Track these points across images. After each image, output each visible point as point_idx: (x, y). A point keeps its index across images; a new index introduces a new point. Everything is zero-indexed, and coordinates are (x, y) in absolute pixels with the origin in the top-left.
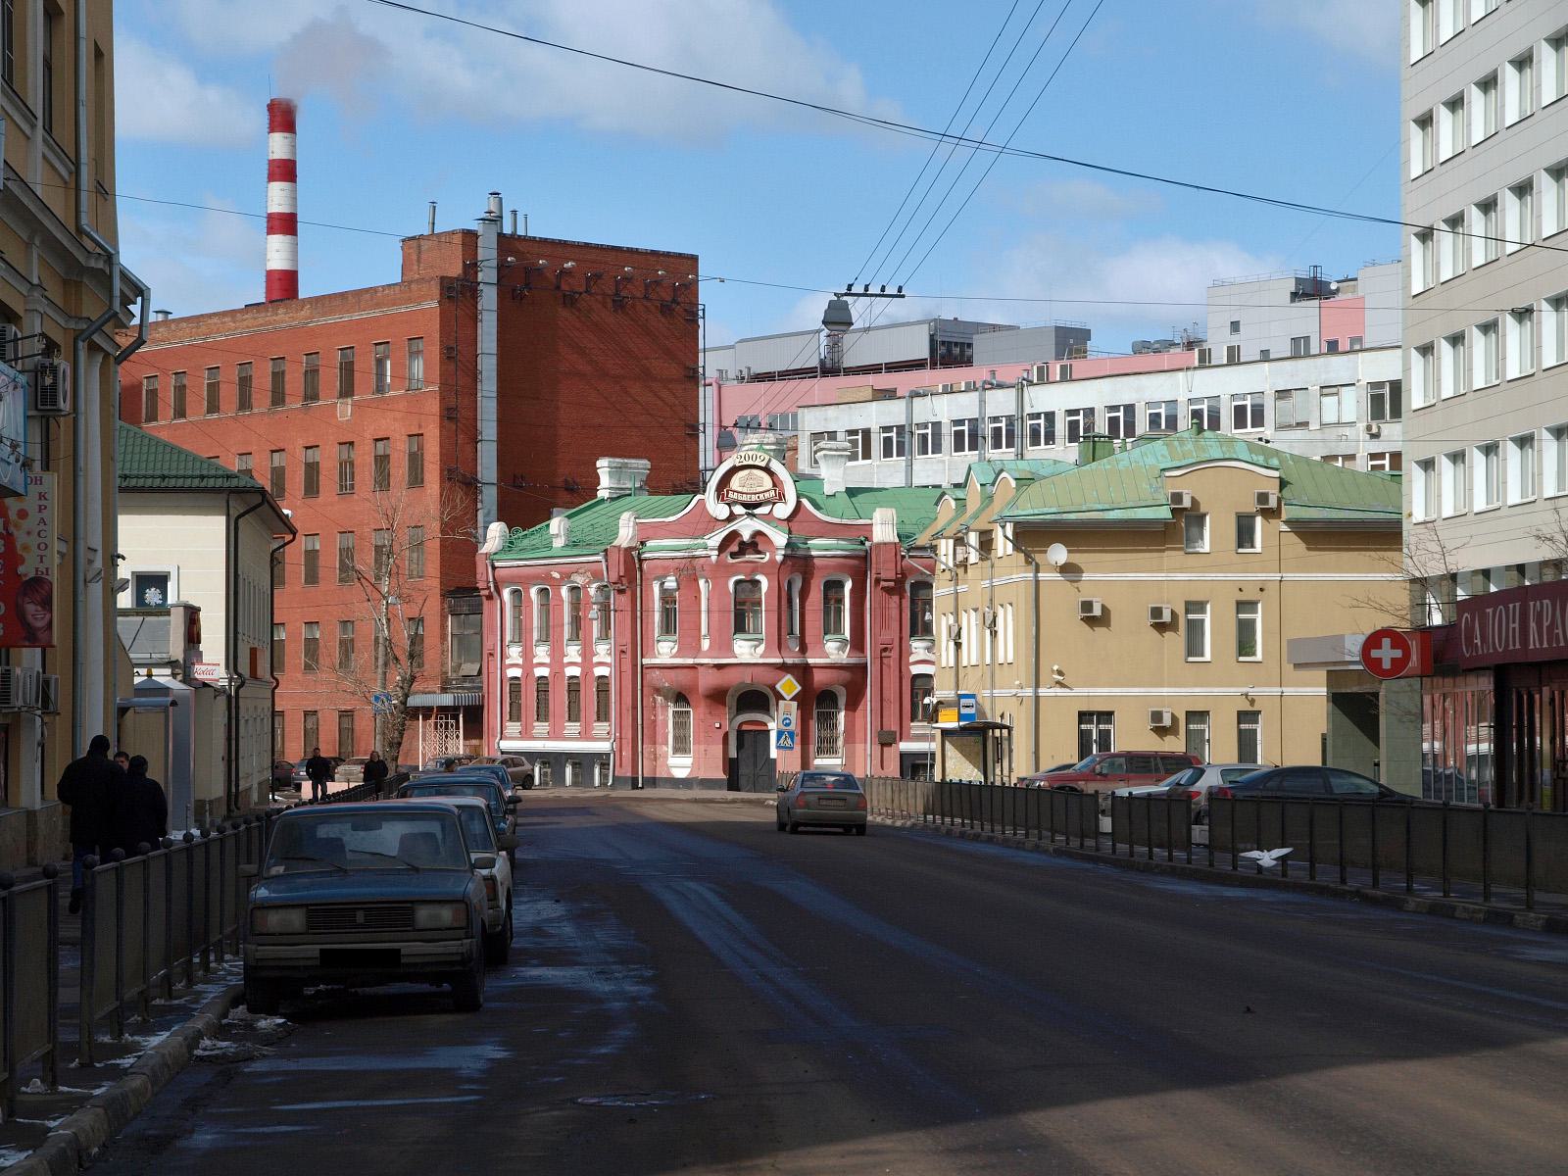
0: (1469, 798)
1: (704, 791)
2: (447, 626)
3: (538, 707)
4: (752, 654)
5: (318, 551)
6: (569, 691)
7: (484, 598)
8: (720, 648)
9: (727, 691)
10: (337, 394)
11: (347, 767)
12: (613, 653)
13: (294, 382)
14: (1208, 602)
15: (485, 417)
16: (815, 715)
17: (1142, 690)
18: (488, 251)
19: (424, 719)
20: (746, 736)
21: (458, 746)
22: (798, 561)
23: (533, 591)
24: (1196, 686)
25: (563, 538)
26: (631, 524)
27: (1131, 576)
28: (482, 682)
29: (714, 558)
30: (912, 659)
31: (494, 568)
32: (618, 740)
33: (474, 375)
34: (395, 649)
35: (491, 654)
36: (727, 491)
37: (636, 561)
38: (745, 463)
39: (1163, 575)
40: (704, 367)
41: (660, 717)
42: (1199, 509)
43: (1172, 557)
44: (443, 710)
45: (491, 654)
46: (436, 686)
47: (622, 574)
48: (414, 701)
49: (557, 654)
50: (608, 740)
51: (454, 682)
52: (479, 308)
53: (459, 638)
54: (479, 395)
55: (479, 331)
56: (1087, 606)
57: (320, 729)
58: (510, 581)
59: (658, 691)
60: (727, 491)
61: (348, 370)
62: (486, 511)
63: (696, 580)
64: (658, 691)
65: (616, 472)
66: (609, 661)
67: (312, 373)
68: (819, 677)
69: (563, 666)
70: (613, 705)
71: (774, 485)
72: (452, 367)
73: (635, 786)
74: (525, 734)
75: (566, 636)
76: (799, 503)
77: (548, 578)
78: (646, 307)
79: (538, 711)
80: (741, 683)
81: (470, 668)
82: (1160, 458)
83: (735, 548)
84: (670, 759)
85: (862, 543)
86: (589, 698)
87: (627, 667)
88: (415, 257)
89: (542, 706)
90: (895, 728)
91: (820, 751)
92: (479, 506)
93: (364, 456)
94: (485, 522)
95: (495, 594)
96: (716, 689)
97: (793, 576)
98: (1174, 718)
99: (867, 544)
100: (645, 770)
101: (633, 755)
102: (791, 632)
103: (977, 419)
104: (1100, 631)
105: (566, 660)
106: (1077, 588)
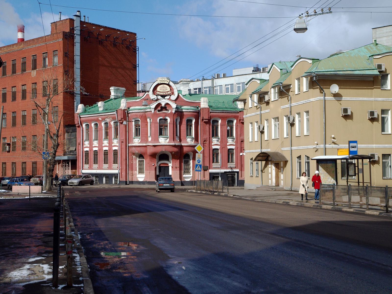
0: (41, 175)
1: (149, 185)
2: (65, 136)
3: (94, 160)
4: (165, 142)
5: (26, 115)
6: (104, 155)
7: (77, 127)
8: (155, 140)
9: (157, 154)
10: (31, 69)
11: (34, 179)
12: (119, 142)
13: (19, 67)
14: (389, 110)
15: (77, 74)
16: (183, 161)
17: (366, 145)
18: (77, 24)
19: (58, 164)
20: (162, 168)
21: (69, 172)
22: (179, 113)
23: (93, 125)
24: (386, 144)
25: (102, 108)
26: (125, 102)
27: (361, 99)
28: (76, 153)
29: (153, 112)
30: (213, 144)
31: (80, 118)
32: (121, 170)
33: (73, 62)
34: (51, 133)
35: (79, 144)
36: (156, 91)
37: (127, 114)
38: (162, 83)
39: (373, 98)
40: (138, 64)
41: (134, 162)
42: (386, 73)
43: (376, 91)
44: (64, 161)
45: (79, 144)
46: (62, 154)
47: (122, 117)
48: (57, 158)
49: (100, 144)
50: (117, 169)
51: (67, 153)
52: (75, 42)
53: (69, 140)
54: (75, 67)
55: (75, 49)
56: (345, 110)
57: (26, 167)
58: (85, 121)
59: (134, 154)
60: (156, 91)
61: (35, 61)
62: (77, 102)
63: (146, 119)
64: (134, 154)
65: (116, 91)
66: (118, 145)
67: (24, 64)
68: (185, 149)
69: (102, 147)
70: (119, 159)
71: (171, 90)
72: (67, 59)
73: (126, 184)
74: (90, 168)
75: (103, 138)
76: (178, 95)
77: (98, 120)
78: (122, 46)
79: (94, 161)
80: (162, 151)
81: (72, 149)
82: (365, 53)
83: (159, 109)
84: (137, 175)
85: (198, 108)
86: (111, 157)
87: (124, 146)
88: (55, 28)
89: (95, 159)
90: (208, 165)
91: (185, 172)
92: (75, 100)
93: (40, 87)
94: (77, 105)
95: (80, 126)
96: (153, 153)
97: (177, 117)
98: (379, 158)
99: (199, 108)
100: (130, 179)
101: (126, 174)
102: (177, 135)
103: (201, 88)
104: (349, 121)
105: (103, 145)
106: (340, 103)
